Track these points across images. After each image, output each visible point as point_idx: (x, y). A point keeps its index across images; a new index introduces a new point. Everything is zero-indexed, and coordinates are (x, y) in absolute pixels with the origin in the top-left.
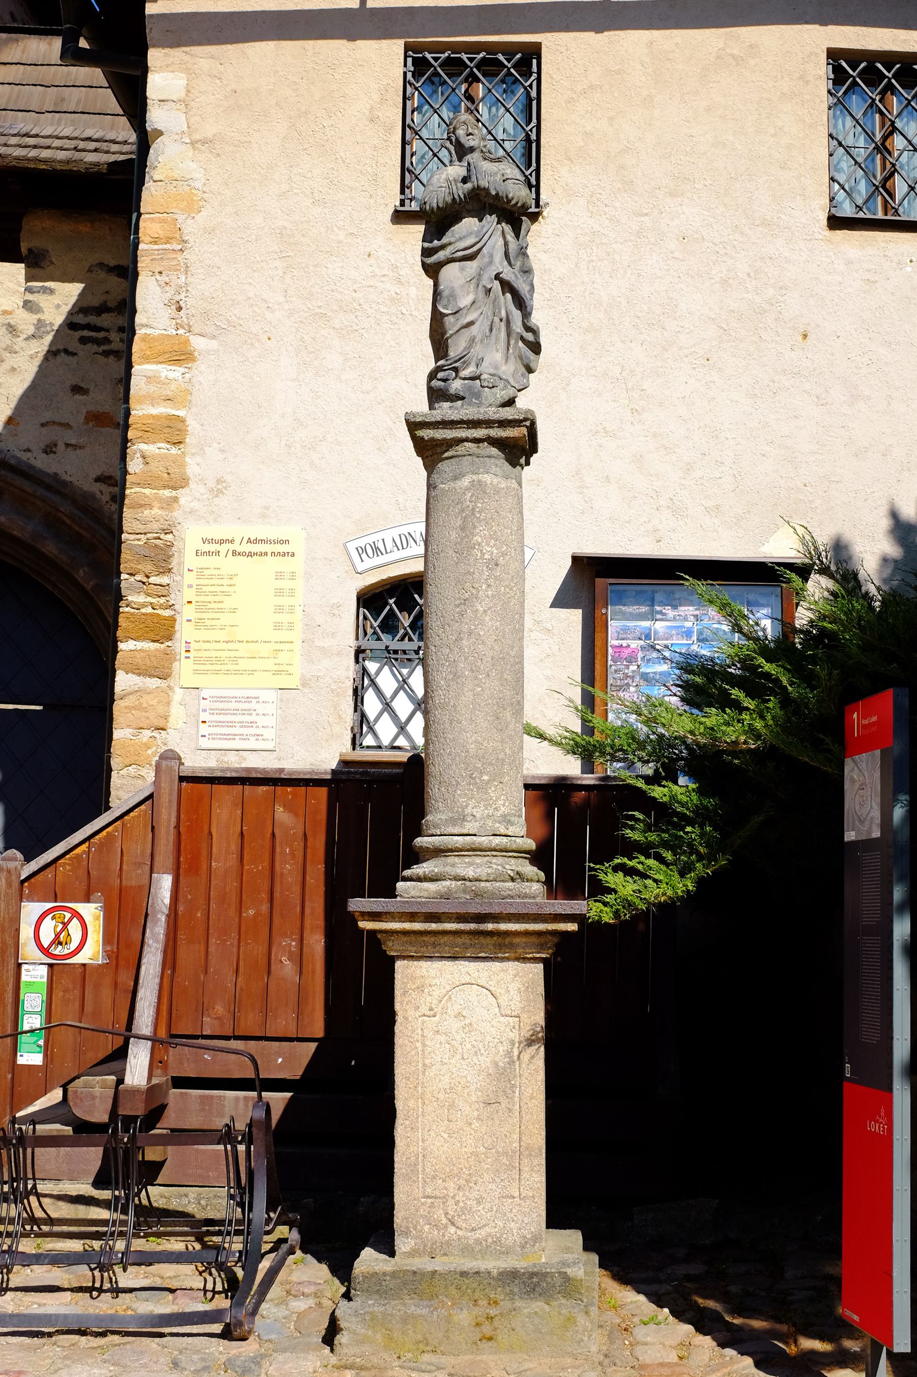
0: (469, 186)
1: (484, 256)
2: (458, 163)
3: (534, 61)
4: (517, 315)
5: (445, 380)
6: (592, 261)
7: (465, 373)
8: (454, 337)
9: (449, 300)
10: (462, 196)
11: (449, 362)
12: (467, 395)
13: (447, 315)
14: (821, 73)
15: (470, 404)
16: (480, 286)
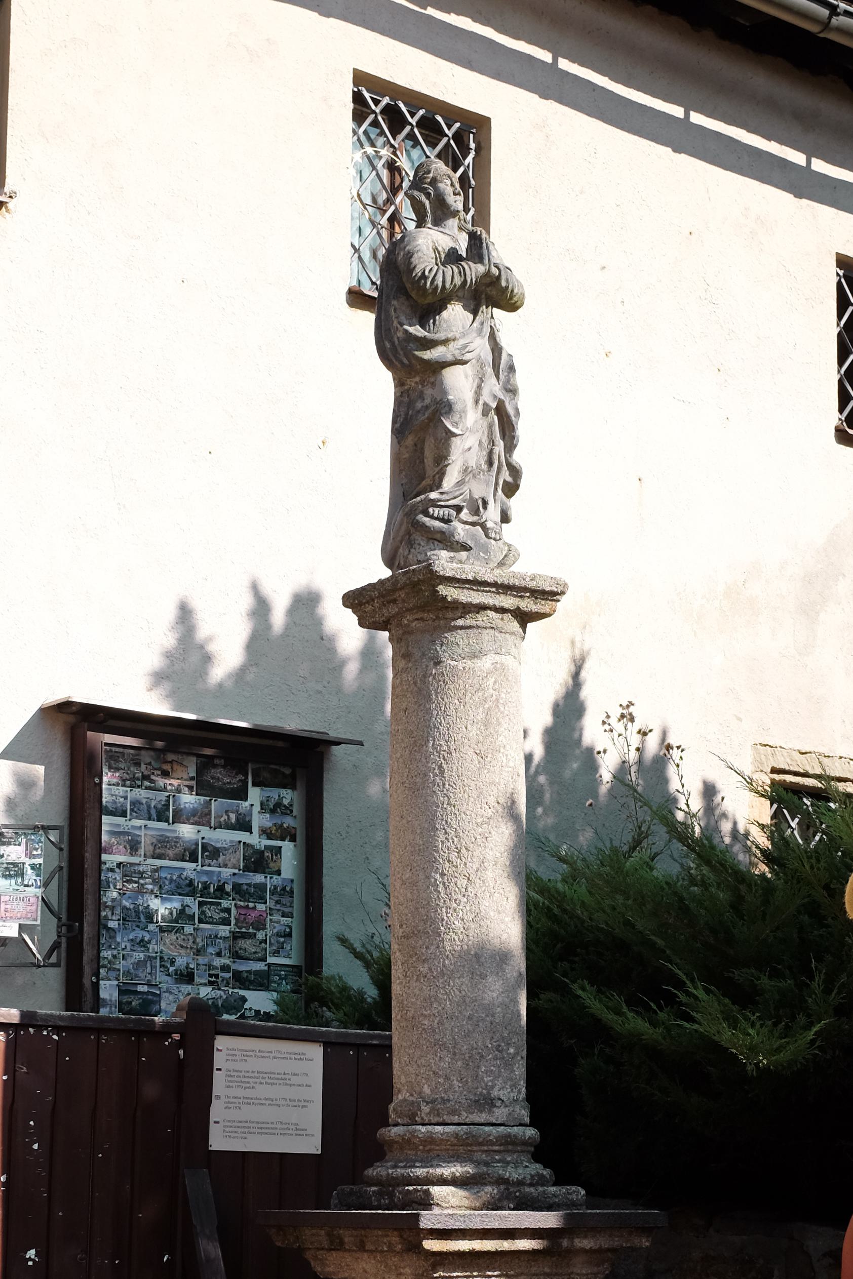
15: (477, 558)
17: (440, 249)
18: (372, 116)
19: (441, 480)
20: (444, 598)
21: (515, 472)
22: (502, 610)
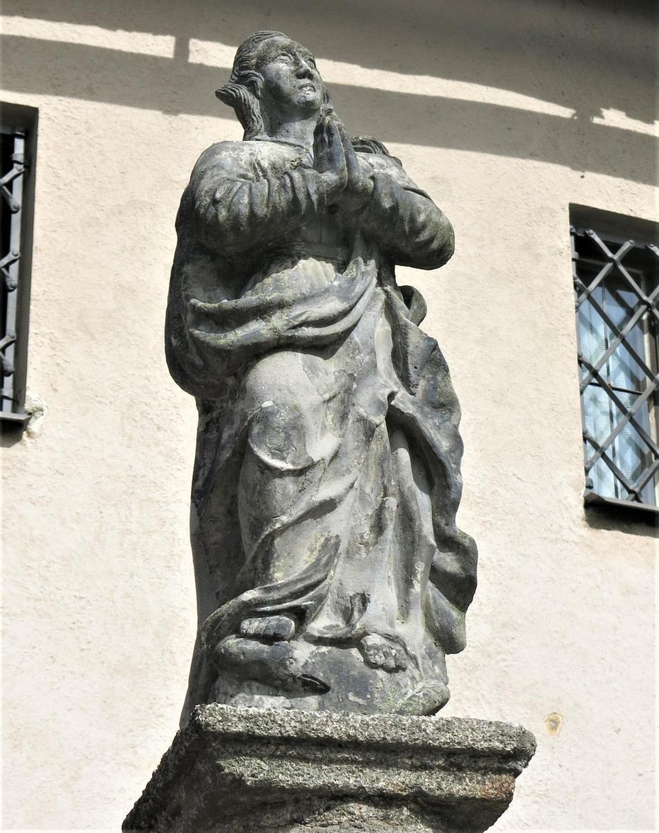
0: (330, 177)
1: (356, 349)
2: (265, 136)
3: (19, 145)
4: (423, 502)
5: (269, 638)
6: (130, 532)
7: (321, 624)
8: (290, 534)
9: (288, 438)
10: (314, 197)
11: (275, 595)
12: (332, 682)
13: (281, 474)
14: (561, 246)
15: (343, 705)
16: (351, 418)
17: (265, 164)
18: (609, 266)
19: (267, 564)
20: (238, 781)
21: (464, 550)
22: (384, 800)
